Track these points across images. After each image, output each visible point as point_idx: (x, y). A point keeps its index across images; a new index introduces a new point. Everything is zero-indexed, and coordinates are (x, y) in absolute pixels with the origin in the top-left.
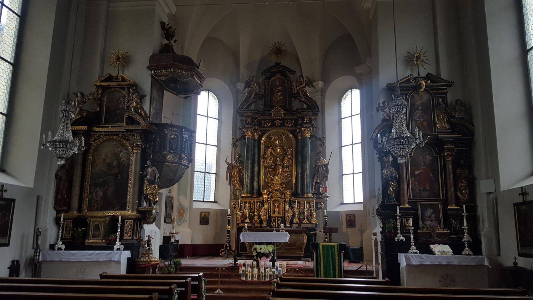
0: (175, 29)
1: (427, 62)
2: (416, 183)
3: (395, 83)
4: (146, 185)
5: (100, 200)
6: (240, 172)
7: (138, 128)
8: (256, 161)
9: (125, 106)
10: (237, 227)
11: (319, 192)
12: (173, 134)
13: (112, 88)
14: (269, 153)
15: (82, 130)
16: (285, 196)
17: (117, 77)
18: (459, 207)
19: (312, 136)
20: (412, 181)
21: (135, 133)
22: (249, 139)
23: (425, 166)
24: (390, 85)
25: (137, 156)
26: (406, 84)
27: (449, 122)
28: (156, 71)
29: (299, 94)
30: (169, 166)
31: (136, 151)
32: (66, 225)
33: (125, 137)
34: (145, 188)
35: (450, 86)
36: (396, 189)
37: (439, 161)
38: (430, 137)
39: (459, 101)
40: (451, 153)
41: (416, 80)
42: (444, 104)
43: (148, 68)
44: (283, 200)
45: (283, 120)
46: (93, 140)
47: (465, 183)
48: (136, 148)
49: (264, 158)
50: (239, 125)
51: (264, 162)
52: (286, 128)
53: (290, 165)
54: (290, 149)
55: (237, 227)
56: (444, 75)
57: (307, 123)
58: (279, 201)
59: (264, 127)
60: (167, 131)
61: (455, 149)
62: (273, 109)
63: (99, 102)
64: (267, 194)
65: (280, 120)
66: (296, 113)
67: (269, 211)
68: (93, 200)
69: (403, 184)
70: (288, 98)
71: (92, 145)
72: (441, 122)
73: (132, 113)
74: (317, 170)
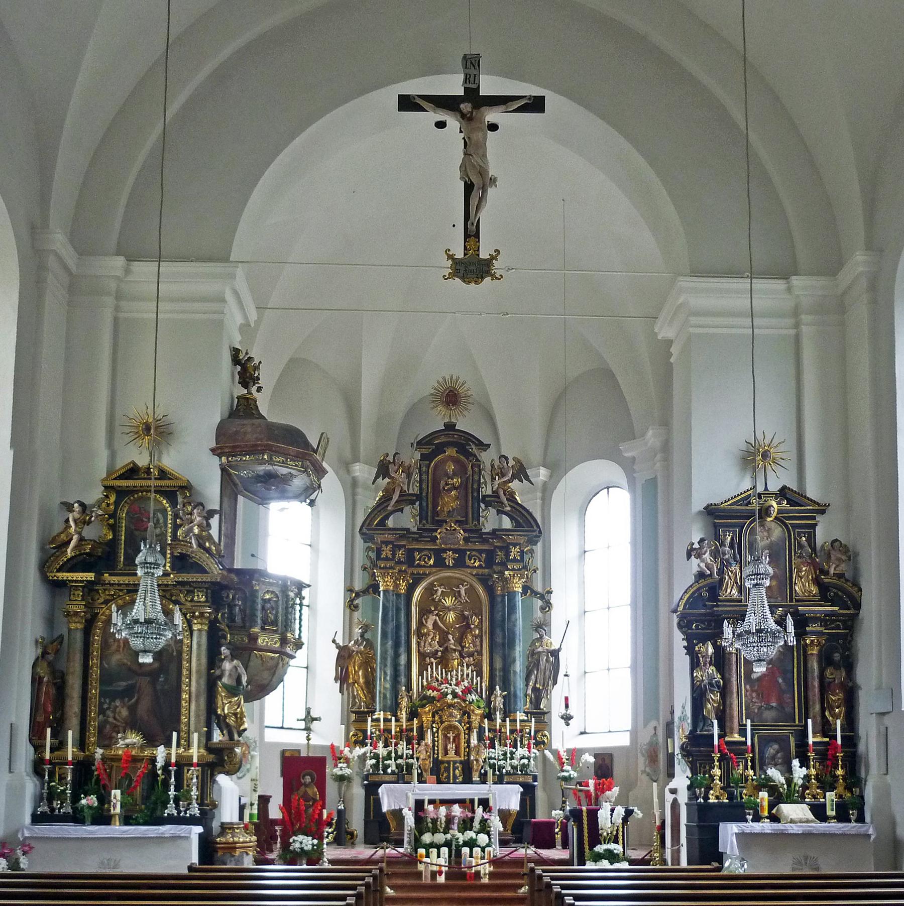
0: (260, 362)
1: (782, 462)
2: (754, 695)
3: (722, 503)
4: (221, 696)
5: (124, 725)
6: (368, 664)
7: (204, 580)
8: (403, 642)
9: (167, 532)
10: (366, 782)
11: (540, 709)
12: (268, 592)
13: (137, 492)
14: (430, 624)
15: (82, 581)
16: (469, 717)
17: (149, 468)
18: (827, 739)
19: (526, 589)
20: (747, 691)
21: (195, 588)
22: (387, 594)
23: (771, 664)
24: (713, 507)
25: (200, 637)
26: (741, 505)
27: (817, 581)
28: (230, 459)
29: (499, 497)
30: (262, 659)
31: (199, 627)
32: (60, 775)
33: (172, 595)
34: (220, 703)
35: (823, 512)
36: (718, 707)
37: (795, 654)
38: (782, 611)
39: (837, 544)
40: (818, 640)
41: (760, 498)
42: (810, 546)
43: (213, 450)
44: (465, 725)
45: (461, 552)
46: (103, 600)
47: (839, 696)
48: (199, 620)
49: (420, 635)
50: (360, 558)
51: (418, 644)
52: (469, 571)
53: (477, 651)
54: (476, 616)
55: (366, 782)
56: (812, 492)
57: (515, 560)
58: (456, 728)
59: (419, 566)
60: (258, 585)
61: (825, 634)
62: (441, 526)
63: (112, 521)
64: (431, 713)
65: (455, 551)
66: (492, 539)
67: (434, 750)
68: (108, 726)
69: (731, 697)
70: (472, 503)
71: (101, 612)
72: (803, 580)
73: (193, 548)
74: (535, 663)
